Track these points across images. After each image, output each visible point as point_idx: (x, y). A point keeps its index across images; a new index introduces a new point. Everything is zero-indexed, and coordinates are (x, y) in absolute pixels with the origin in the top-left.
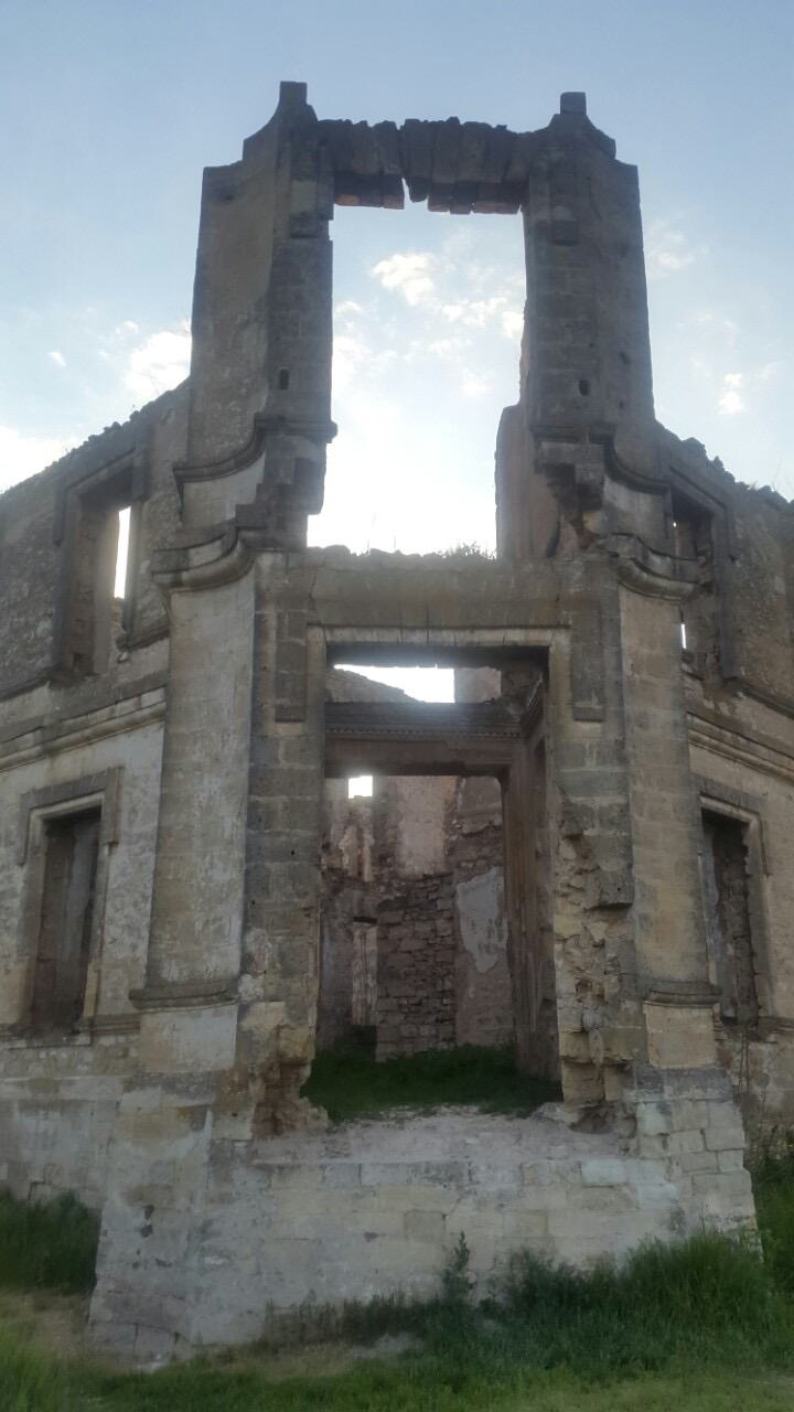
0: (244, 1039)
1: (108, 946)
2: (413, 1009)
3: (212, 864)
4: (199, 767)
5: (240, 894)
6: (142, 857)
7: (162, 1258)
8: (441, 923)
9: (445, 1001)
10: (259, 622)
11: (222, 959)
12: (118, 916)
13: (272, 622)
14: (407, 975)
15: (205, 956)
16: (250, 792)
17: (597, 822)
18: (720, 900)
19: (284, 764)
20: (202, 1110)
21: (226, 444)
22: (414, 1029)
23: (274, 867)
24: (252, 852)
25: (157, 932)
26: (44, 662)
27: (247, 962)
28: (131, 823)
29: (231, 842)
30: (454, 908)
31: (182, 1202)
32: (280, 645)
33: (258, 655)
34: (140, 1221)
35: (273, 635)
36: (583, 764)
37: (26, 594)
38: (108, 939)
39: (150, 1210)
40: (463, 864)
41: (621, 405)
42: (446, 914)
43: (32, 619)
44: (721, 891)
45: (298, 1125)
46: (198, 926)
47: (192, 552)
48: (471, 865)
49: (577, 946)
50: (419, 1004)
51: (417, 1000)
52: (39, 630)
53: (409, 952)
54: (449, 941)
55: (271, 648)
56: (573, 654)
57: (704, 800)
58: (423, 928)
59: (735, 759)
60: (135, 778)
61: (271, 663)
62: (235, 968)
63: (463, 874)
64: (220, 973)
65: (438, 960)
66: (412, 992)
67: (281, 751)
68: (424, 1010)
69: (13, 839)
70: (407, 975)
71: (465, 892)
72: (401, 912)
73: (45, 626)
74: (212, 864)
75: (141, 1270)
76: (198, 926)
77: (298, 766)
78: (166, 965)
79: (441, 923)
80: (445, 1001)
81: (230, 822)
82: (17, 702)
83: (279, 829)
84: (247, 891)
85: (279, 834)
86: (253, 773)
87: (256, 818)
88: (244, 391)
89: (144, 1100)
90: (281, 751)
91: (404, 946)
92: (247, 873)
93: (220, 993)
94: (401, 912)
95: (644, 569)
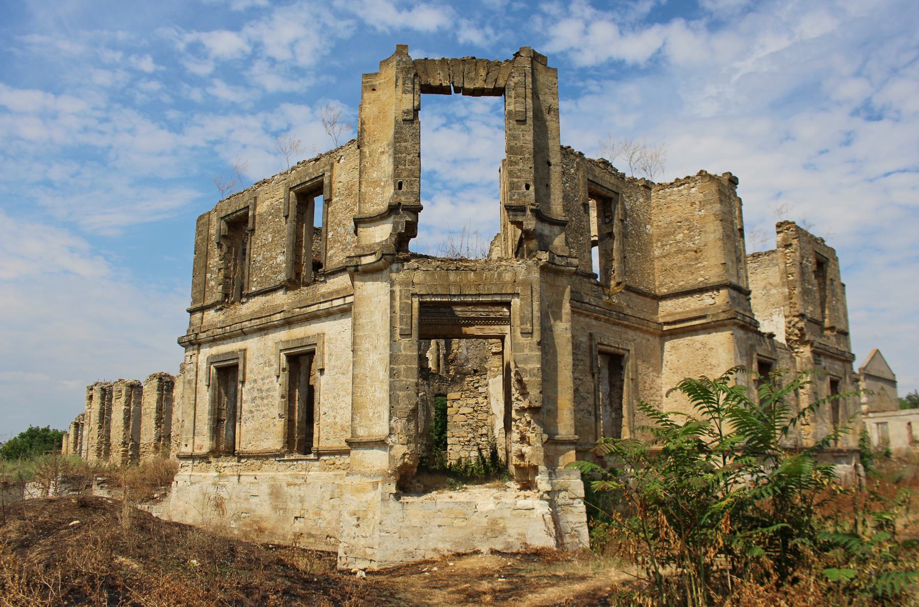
0: (392, 458)
1: (322, 416)
2: (466, 443)
3: (375, 390)
4: (368, 350)
5: (387, 403)
6: (336, 377)
7: (364, 535)
8: (480, 399)
9: (483, 439)
10: (392, 293)
11: (380, 429)
12: (326, 402)
13: (398, 294)
14: (463, 426)
15: (374, 426)
16: (390, 364)
17: (528, 375)
18: (610, 391)
19: (404, 353)
20: (377, 483)
21: (375, 207)
22: (467, 453)
23: (401, 393)
24: (392, 388)
25: (354, 417)
26: (282, 277)
27: (391, 431)
28: (330, 360)
29: (382, 382)
30: (487, 392)
31: (370, 515)
32: (401, 303)
33: (392, 307)
34: (355, 522)
35: (398, 298)
36: (523, 351)
37: (270, 240)
38: (322, 413)
39: (358, 519)
40: (492, 369)
41: (547, 186)
42: (484, 395)
43: (274, 254)
44: (610, 387)
45: (412, 489)
46: (371, 414)
47: (362, 258)
48: (496, 369)
49: (520, 422)
50: (469, 441)
51: (468, 439)
52: (278, 260)
53: (464, 414)
54: (485, 409)
55: (397, 304)
56: (521, 305)
57: (600, 346)
58: (472, 401)
59: (618, 324)
60: (330, 339)
61: (397, 309)
62: (387, 432)
63: (492, 374)
64: (381, 433)
65: (479, 418)
66: (465, 435)
67: (402, 347)
68: (473, 443)
69: (272, 363)
70: (463, 426)
71: (494, 383)
72: (460, 393)
73: (281, 258)
74: (375, 390)
75: (356, 539)
76: (371, 414)
77: (409, 353)
78: (359, 430)
79: (480, 399)
80: (483, 439)
81: (382, 374)
82: (269, 298)
83: (402, 378)
84: (390, 403)
85: (402, 381)
86: (391, 356)
87: (393, 374)
88: (382, 184)
89: (356, 480)
90: (402, 347)
91: (462, 411)
92: (390, 396)
93: (381, 444)
94: (460, 393)
95: (553, 264)
